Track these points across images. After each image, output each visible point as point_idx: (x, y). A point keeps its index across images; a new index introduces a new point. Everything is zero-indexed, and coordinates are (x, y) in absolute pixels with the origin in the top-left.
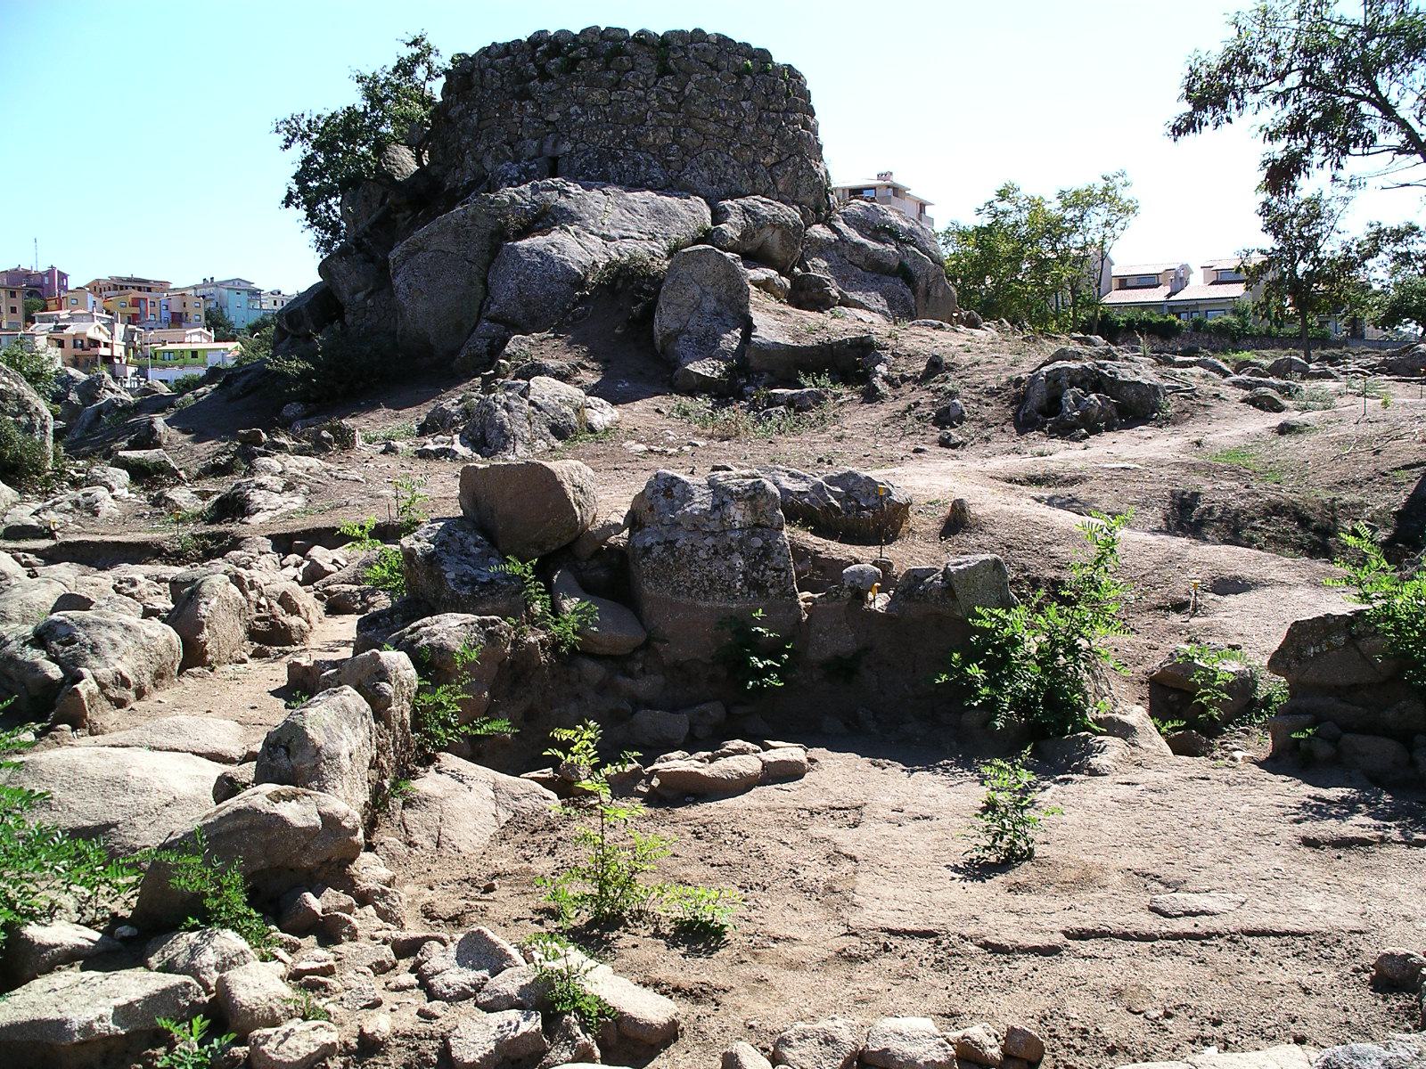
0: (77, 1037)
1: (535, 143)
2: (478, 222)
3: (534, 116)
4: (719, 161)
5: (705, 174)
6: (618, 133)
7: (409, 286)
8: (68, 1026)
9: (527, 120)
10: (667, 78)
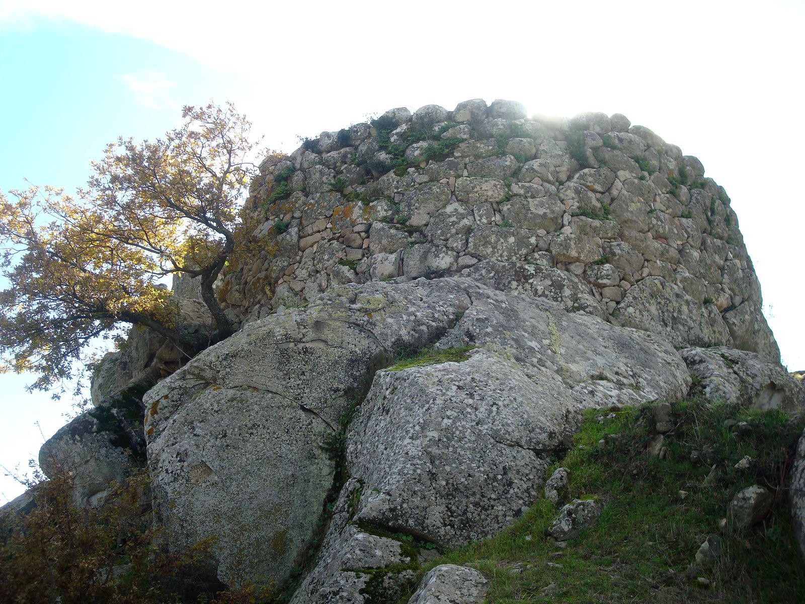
0: (98, 412)
1: (392, 257)
2: (327, 334)
3: (388, 220)
4: (668, 292)
5: (653, 309)
6: (522, 242)
7: (182, 457)
8: (113, 437)
9: (378, 225)
10: (586, 171)
